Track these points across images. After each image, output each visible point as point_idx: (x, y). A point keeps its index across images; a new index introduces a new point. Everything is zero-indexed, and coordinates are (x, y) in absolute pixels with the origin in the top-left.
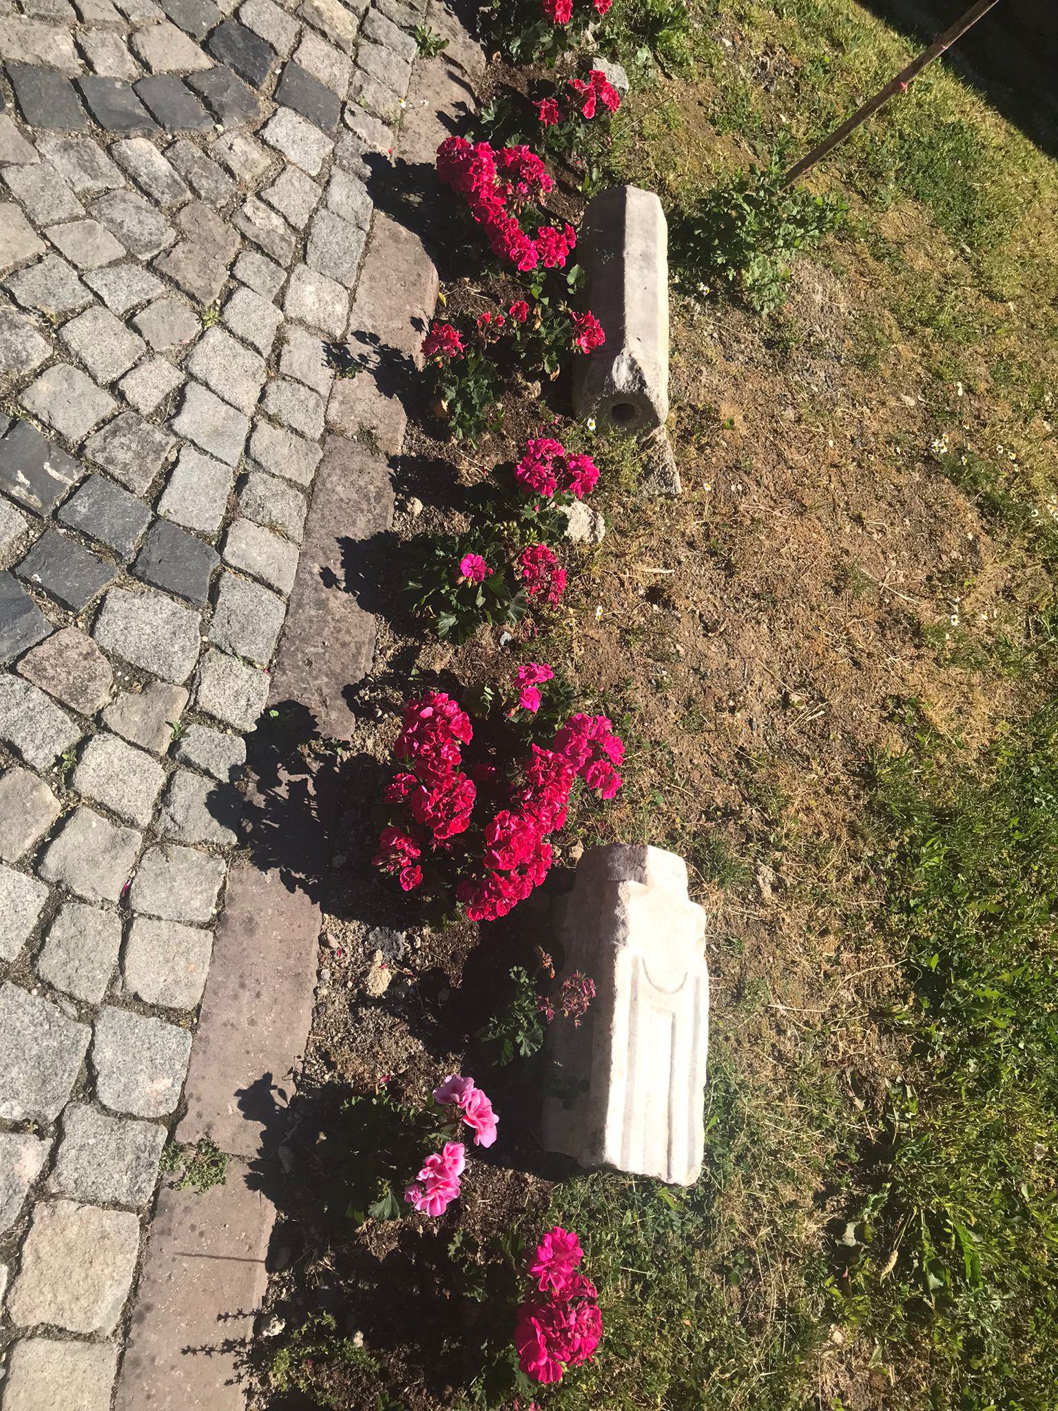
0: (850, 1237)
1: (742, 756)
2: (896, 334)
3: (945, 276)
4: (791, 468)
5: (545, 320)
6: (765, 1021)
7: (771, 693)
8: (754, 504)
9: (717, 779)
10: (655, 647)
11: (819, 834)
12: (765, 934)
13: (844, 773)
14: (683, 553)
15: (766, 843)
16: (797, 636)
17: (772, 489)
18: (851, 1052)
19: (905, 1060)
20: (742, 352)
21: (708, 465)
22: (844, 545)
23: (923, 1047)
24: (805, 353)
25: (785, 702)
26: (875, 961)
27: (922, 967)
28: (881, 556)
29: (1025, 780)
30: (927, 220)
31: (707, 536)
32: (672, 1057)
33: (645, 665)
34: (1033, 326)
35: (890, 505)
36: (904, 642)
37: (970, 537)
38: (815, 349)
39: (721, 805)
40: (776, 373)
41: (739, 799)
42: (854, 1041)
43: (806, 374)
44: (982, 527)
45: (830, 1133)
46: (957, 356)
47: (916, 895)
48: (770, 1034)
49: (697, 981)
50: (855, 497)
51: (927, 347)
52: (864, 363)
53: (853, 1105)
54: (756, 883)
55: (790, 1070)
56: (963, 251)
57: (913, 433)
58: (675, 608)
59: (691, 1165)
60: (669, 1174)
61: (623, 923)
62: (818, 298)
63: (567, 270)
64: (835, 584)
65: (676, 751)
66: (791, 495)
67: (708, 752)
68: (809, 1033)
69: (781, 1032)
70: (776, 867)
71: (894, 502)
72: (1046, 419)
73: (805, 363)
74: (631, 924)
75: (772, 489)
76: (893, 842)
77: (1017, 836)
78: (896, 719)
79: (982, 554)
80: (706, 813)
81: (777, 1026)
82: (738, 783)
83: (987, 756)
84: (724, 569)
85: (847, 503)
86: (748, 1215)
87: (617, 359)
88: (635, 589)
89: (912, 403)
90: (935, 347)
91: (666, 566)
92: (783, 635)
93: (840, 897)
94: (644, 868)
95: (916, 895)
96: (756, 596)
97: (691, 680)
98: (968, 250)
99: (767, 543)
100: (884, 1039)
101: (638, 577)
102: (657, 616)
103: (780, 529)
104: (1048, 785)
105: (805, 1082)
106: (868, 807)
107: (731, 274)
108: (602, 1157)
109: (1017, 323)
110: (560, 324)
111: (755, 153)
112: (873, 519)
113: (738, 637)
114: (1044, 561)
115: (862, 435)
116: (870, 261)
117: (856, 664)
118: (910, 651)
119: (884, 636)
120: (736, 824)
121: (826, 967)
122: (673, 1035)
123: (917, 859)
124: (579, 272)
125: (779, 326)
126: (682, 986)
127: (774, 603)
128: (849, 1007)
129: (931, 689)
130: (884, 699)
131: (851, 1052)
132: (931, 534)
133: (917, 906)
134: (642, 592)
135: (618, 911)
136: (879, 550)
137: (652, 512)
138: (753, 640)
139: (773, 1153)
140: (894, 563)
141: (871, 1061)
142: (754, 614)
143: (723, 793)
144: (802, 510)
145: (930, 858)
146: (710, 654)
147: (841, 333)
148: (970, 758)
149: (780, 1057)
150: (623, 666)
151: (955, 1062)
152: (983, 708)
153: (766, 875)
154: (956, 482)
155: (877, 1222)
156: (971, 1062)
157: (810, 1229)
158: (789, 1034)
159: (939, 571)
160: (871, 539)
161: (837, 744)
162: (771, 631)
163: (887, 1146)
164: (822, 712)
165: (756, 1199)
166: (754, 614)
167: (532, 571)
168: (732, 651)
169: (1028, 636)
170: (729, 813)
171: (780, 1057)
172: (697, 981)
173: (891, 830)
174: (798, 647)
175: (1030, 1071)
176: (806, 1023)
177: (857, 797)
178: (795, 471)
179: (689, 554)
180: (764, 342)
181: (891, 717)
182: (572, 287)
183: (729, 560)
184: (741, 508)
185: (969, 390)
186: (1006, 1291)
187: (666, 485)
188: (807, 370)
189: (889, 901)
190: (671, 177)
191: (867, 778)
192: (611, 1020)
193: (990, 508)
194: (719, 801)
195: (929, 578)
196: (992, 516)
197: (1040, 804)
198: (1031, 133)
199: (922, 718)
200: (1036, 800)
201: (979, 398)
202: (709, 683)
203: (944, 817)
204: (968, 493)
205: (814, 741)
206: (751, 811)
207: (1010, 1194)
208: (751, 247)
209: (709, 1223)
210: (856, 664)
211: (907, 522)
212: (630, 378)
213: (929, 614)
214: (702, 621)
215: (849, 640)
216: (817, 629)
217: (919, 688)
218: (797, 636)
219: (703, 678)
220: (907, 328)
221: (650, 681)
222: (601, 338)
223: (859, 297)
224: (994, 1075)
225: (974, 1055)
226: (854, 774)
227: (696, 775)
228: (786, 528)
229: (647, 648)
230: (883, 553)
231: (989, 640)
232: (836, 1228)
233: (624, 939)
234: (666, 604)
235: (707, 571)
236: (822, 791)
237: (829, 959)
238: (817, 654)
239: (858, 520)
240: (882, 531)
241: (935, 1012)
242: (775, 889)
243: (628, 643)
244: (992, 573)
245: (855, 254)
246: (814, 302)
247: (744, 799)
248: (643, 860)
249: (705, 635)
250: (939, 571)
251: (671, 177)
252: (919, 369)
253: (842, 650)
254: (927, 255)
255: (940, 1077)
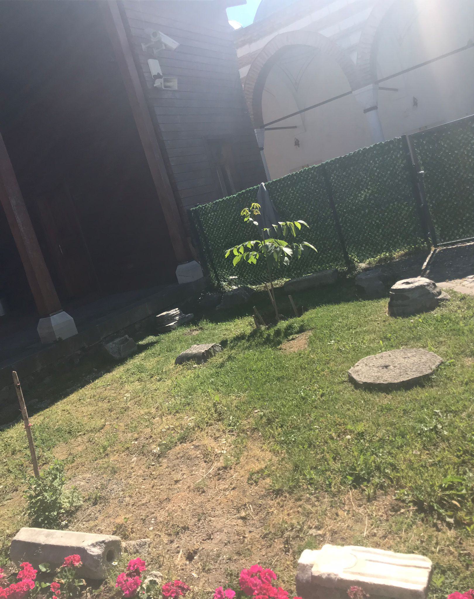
0: (451, 520)
1: (265, 537)
2: (106, 460)
3: (88, 442)
4: (150, 501)
5: (62, 577)
6: (371, 540)
7: (240, 522)
8: (162, 515)
9: (272, 546)
10: (213, 559)
11: (298, 512)
12: (337, 536)
13: (276, 501)
14: (175, 545)
15: (301, 530)
16: (218, 508)
17: (156, 509)
18: (383, 511)
19: (386, 494)
20: (95, 514)
21: (141, 530)
22: (186, 487)
23: (382, 487)
24: (104, 491)
25: (243, 518)
26: (349, 499)
27: (352, 483)
28: (193, 476)
29: (286, 443)
30: (64, 445)
31: (170, 535)
32: (383, 563)
33: (220, 564)
34: (117, 418)
35: (173, 470)
36: (228, 472)
37: (193, 447)
38: (103, 487)
39: (283, 546)
40: (109, 502)
41: (281, 539)
42: (379, 510)
43: (113, 492)
44: (190, 443)
45: (414, 523)
46: (122, 441)
47: (325, 481)
48: (376, 539)
49: (353, 550)
50: (168, 482)
51: (115, 451)
52: (114, 472)
53: (403, 513)
54: (316, 536)
55: (390, 533)
56: (81, 435)
57: (147, 459)
58: (198, 549)
59: (424, 560)
60: (428, 568)
61: (329, 575)
62: (82, 483)
63: (40, 571)
64: (200, 492)
65: (259, 561)
66: (161, 502)
67: (261, 549)
68: (375, 525)
69: (375, 535)
70: (310, 528)
71: (173, 469)
72: (154, 418)
73: (108, 491)
74: (329, 571)
75: (156, 509)
76: (304, 486)
77: (306, 446)
78: (257, 480)
79: (200, 444)
80: (286, 552)
81: (373, 536)
82: (275, 539)
83: (275, 453)
84: (185, 530)
85: (169, 485)
86: (446, 554)
87: (88, 552)
88: (186, 565)
89: (135, 458)
90: (115, 448)
91: (178, 552)
92: (217, 513)
93: (324, 507)
94: (307, 565)
95: (325, 481)
96: (199, 520)
97: (229, 547)
98: (81, 433)
99: (178, 513)
100: (378, 499)
101: (181, 563)
102: (200, 557)
103: (174, 508)
104: (288, 435)
105: (394, 528)
106: (290, 493)
107: (62, 511)
108: (421, 592)
109: (115, 422)
110: (66, 572)
111: (10, 499)
112: (179, 476)
113: (215, 527)
114: (207, 426)
115: (143, 476)
116: (73, 465)
117: (234, 489)
118: (232, 471)
119: (225, 478)
120: (291, 541)
121: (350, 515)
122: (374, 561)
123: (311, 479)
124: (43, 566)
125: (89, 499)
126: (355, 556)
127: (203, 514)
128: (366, 509)
129: (247, 468)
130: (249, 484)
131: (383, 511)
132: (188, 459)
133: (329, 482)
134: (188, 562)
135: (324, 577)
136: (190, 477)
137: (154, 552)
138: (217, 523)
139: (422, 542)
140: (197, 472)
141: (386, 505)
142: (206, 522)
143: (279, 545)
144: (168, 500)
145: (311, 474)
146: (220, 538)
147: (99, 478)
148: (275, 459)
149: (385, 537)
150: (219, 572)
151: (386, 476)
152: (258, 452)
153: (313, 532)
154: (170, 449)
155: (446, 511)
156: (387, 471)
157: (451, 533)
158: (376, 532)
159: (203, 458)
160: (185, 479)
161: (264, 502)
162: (214, 517)
163: (418, 503)
164: (250, 506)
165: (439, 551)
166: (206, 522)
167: (172, 593)
168: (221, 531)
169: (234, 435)
170: (287, 542)
171: (385, 537)
172: (353, 550)
173: (300, 487)
174: (223, 508)
175: (390, 453)
176: (372, 525)
177: (286, 497)
178: (151, 500)
179: (175, 543)
180: (93, 506)
181: (256, 482)
182: (47, 570)
183: (182, 528)
184: (162, 520)
185: (136, 439)
186: (466, 471)
187: (145, 545)
188: (111, 491)
189: (326, 491)
190: (7, 531)
191: (278, 493)
192: (367, 583)
193: (183, 439)
194: (282, 546)
195: (205, 462)
196: (186, 439)
197: (295, 439)
198: (42, 409)
199: (258, 472)
200: (293, 440)
201: (140, 437)
202: (232, 541)
203: (296, 468)
204: (176, 446)
205: (261, 510)
206: (287, 534)
207: (433, 465)
208: (56, 499)
209: (450, 569)
210: (234, 489)
211: (182, 466)
212: (99, 547)
213: (219, 463)
214: (205, 540)
215: (224, 490)
216: (217, 500)
217: (246, 472)
218: (218, 508)
219: (229, 542)
220: (105, 456)
221: (227, 562)
222: (78, 557)
223: (87, 470)
224: (392, 465)
225: (384, 469)
226: (276, 497)
227: (269, 554)
228: (174, 506)
229: (212, 562)
230: (192, 475)
231: (233, 446)
232: (449, 525)
233: (335, 575)
234: (195, 553)
235: (184, 537)
236: (282, 509)
237: (347, 514)
238: (227, 502)
239: (177, 482)
240: (183, 474)
241: (368, 481)
242: (319, 529)
243: (209, 570)
244: (208, 442)
245: (68, 469)
246: (83, 485)
247: (282, 537)
248: (304, 565)
249: (212, 539)
250: (203, 458)
251: (7, 531)
252: (123, 454)
253: (227, 493)
254: (77, 446)
255: (392, 482)
